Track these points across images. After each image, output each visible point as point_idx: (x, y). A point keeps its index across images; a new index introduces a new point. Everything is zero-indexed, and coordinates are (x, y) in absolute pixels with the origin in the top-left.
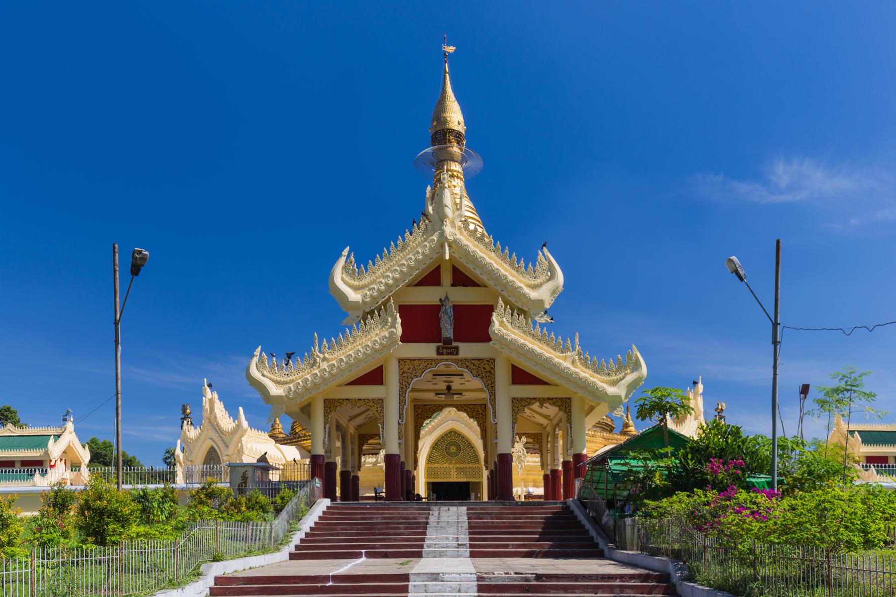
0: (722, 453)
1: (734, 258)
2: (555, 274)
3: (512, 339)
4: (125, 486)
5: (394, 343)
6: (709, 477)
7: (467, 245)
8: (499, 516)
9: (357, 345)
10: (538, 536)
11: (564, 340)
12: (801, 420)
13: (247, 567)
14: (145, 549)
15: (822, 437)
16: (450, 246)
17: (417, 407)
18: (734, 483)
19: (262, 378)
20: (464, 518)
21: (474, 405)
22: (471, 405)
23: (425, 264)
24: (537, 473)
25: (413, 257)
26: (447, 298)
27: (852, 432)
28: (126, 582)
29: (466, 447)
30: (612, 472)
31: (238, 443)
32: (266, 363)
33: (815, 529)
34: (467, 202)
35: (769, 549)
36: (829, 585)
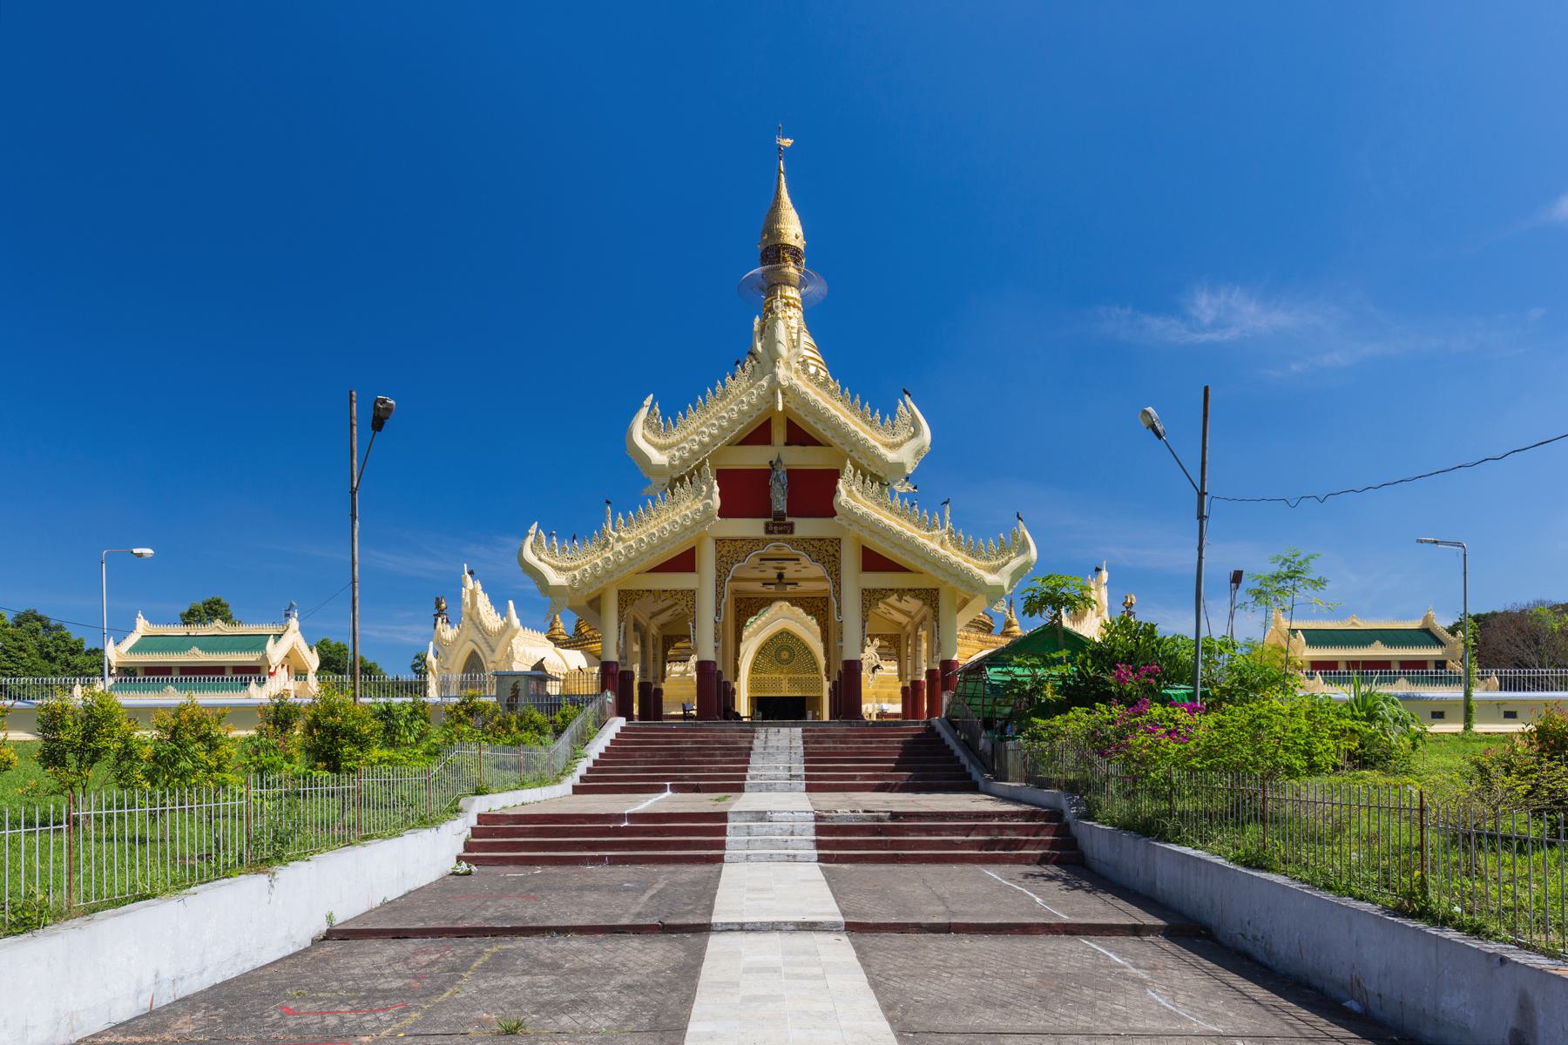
0: (1131, 658)
1: (1150, 409)
2: (920, 430)
4: (362, 700)
5: (709, 518)
6: (1113, 688)
8: (844, 739)
10: (893, 765)
11: (931, 515)
12: (1232, 616)
13: (519, 803)
14: (389, 777)
15: (1258, 637)
16: (784, 394)
18: (1146, 695)
19: (539, 562)
21: (812, 598)
24: (894, 685)
25: (735, 408)
27: (1294, 631)
28: (365, 819)
30: (990, 683)
31: (507, 646)
32: (544, 543)
33: (1248, 752)
34: (806, 338)
35: (1189, 777)
36: (1263, 820)
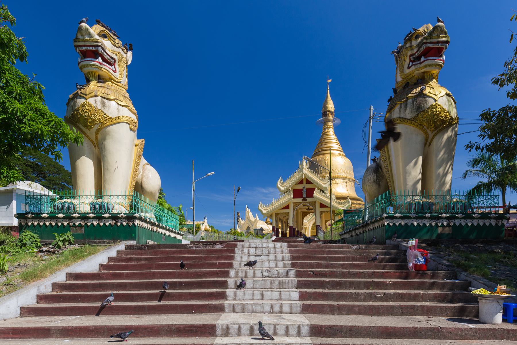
16: (305, 175)
17: (303, 213)
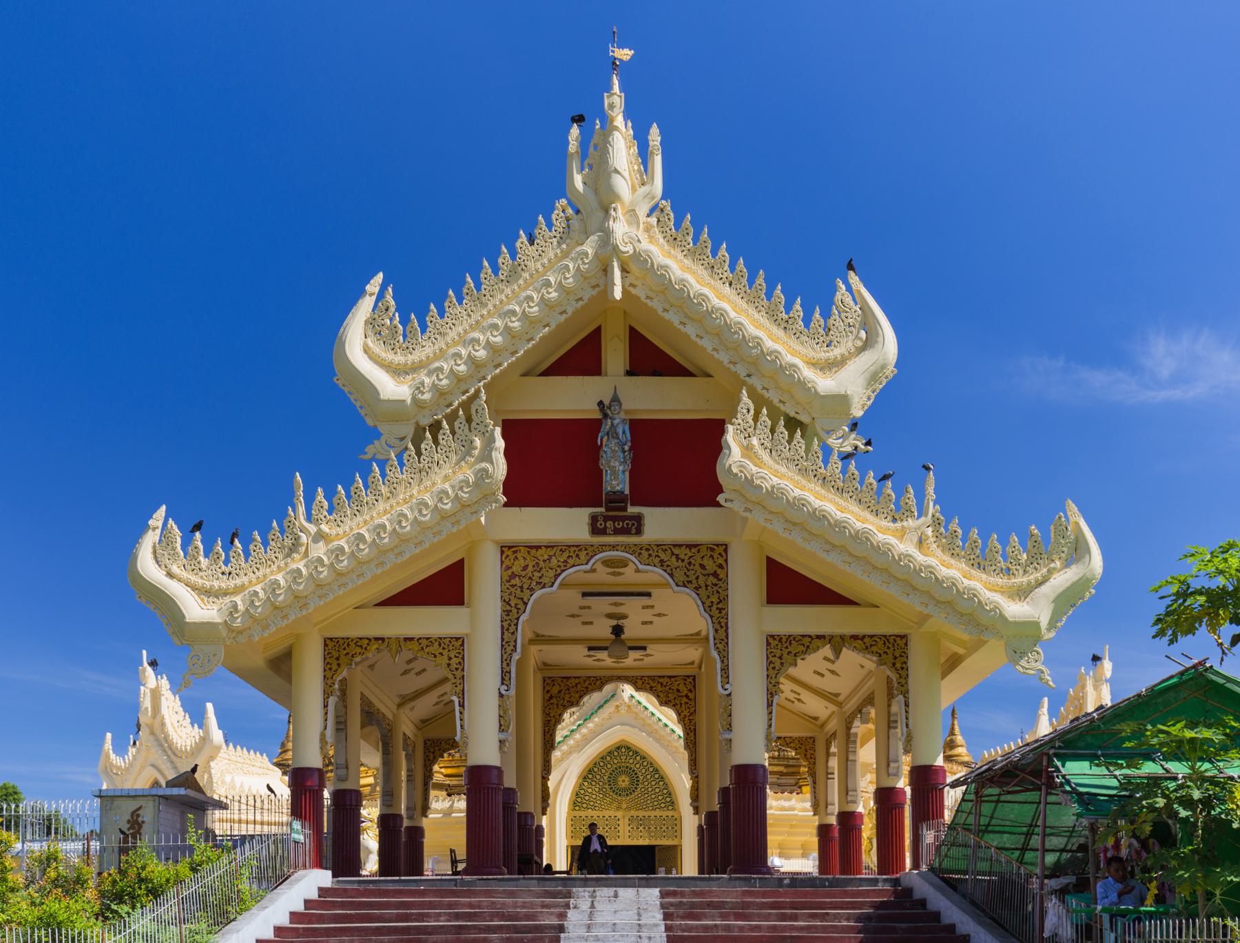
2: (877, 335)
3: (773, 487)
7: (667, 266)
9: (398, 503)
16: (624, 270)
17: (548, 682)
20: (654, 917)
21: (670, 677)
22: (663, 677)
23: (564, 312)
24: (787, 829)
26: (615, 399)
29: (649, 777)
30: (1074, 791)
32: (178, 545)
